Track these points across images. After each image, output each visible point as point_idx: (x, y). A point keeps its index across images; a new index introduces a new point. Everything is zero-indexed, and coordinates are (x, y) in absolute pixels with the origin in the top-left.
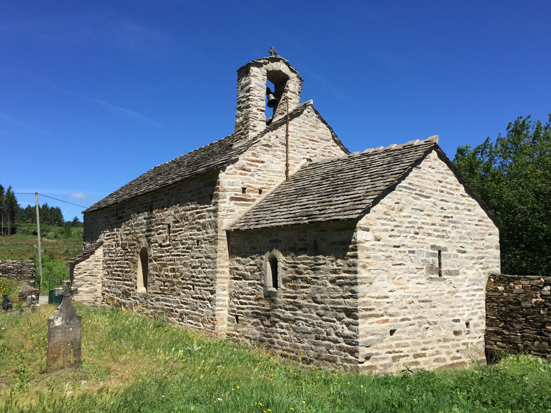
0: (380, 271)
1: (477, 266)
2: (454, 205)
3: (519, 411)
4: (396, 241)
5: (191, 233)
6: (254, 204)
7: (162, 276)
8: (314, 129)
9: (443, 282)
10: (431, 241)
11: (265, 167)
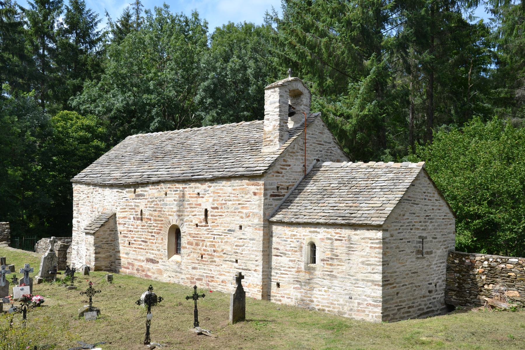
1: (443, 247)
4: (401, 236)
5: (233, 219)
10: (418, 233)
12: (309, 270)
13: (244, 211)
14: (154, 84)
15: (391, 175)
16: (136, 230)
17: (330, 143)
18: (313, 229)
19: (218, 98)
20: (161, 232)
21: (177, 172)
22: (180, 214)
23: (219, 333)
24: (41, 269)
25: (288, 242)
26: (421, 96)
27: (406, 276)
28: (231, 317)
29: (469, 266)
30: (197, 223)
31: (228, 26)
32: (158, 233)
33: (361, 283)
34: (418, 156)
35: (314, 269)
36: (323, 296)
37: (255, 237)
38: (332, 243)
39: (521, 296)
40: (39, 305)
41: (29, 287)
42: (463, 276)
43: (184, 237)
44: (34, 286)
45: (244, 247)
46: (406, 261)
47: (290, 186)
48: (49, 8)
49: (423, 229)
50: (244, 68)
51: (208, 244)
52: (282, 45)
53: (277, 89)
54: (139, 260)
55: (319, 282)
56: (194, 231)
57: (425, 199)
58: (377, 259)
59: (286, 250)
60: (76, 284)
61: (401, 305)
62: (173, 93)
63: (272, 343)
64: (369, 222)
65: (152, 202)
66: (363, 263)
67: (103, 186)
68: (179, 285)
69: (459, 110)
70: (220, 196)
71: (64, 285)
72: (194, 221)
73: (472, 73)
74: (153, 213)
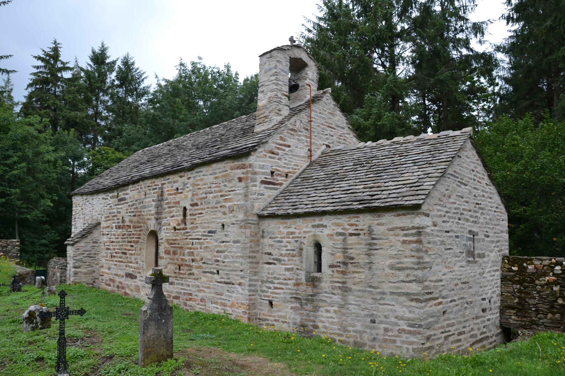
0: (437, 255)
1: (496, 249)
2: (482, 193)
4: (447, 226)
5: (214, 216)
6: (281, 188)
7: (177, 259)
8: (331, 116)
9: (476, 265)
10: (469, 226)
11: (291, 151)
13: (228, 204)
15: (426, 148)
16: (117, 240)
17: (343, 128)
25: (284, 243)
27: (454, 287)
29: (533, 273)
30: (175, 225)
33: (390, 297)
36: (332, 320)
37: (240, 239)
38: (344, 240)
42: (526, 287)
43: (162, 245)
45: (226, 253)
46: (455, 264)
47: (290, 172)
49: (473, 222)
55: (326, 299)
57: (475, 180)
59: (281, 255)
61: (450, 331)
65: (132, 206)
66: (392, 267)
70: (200, 189)
72: (171, 224)
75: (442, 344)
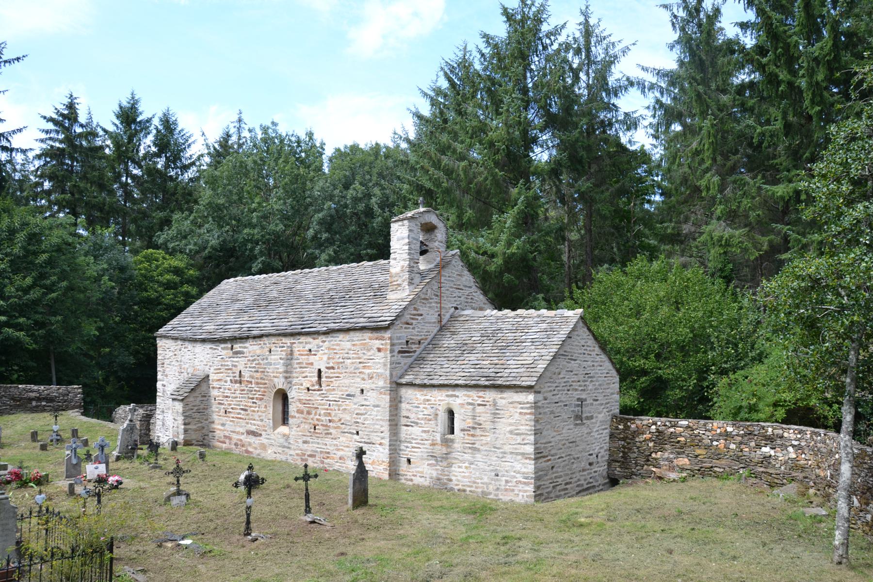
1: (605, 410)
3: (348, 578)
10: (577, 395)
12: (446, 442)
13: (367, 371)
14: (257, 217)
15: (544, 326)
17: (470, 287)
18: (450, 393)
19: (336, 233)
20: (265, 398)
21: (283, 324)
22: (288, 375)
23: (335, 522)
24: (119, 443)
26: (579, 231)
28: (350, 501)
31: (351, 146)
32: (261, 399)
34: (576, 303)
35: (452, 441)
38: (474, 409)
39: (691, 464)
40: (116, 487)
41: (104, 465)
42: (628, 443)
44: (110, 464)
48: (135, 129)
50: (368, 196)
51: (323, 412)
52: (413, 169)
53: (406, 222)
54: (238, 433)
56: (304, 396)
58: (528, 427)
60: (161, 462)
62: (281, 227)
63: (401, 532)
64: (518, 383)
65: (253, 361)
66: (511, 432)
67: (195, 341)
68: (286, 462)
69: (622, 248)
71: (146, 463)
73: (635, 205)
74: (255, 374)
75: (551, 492)
